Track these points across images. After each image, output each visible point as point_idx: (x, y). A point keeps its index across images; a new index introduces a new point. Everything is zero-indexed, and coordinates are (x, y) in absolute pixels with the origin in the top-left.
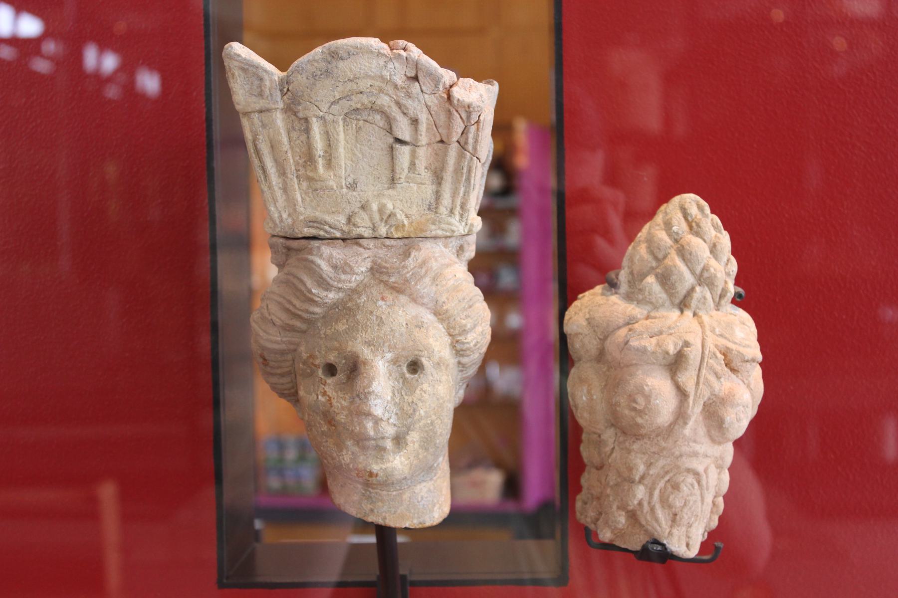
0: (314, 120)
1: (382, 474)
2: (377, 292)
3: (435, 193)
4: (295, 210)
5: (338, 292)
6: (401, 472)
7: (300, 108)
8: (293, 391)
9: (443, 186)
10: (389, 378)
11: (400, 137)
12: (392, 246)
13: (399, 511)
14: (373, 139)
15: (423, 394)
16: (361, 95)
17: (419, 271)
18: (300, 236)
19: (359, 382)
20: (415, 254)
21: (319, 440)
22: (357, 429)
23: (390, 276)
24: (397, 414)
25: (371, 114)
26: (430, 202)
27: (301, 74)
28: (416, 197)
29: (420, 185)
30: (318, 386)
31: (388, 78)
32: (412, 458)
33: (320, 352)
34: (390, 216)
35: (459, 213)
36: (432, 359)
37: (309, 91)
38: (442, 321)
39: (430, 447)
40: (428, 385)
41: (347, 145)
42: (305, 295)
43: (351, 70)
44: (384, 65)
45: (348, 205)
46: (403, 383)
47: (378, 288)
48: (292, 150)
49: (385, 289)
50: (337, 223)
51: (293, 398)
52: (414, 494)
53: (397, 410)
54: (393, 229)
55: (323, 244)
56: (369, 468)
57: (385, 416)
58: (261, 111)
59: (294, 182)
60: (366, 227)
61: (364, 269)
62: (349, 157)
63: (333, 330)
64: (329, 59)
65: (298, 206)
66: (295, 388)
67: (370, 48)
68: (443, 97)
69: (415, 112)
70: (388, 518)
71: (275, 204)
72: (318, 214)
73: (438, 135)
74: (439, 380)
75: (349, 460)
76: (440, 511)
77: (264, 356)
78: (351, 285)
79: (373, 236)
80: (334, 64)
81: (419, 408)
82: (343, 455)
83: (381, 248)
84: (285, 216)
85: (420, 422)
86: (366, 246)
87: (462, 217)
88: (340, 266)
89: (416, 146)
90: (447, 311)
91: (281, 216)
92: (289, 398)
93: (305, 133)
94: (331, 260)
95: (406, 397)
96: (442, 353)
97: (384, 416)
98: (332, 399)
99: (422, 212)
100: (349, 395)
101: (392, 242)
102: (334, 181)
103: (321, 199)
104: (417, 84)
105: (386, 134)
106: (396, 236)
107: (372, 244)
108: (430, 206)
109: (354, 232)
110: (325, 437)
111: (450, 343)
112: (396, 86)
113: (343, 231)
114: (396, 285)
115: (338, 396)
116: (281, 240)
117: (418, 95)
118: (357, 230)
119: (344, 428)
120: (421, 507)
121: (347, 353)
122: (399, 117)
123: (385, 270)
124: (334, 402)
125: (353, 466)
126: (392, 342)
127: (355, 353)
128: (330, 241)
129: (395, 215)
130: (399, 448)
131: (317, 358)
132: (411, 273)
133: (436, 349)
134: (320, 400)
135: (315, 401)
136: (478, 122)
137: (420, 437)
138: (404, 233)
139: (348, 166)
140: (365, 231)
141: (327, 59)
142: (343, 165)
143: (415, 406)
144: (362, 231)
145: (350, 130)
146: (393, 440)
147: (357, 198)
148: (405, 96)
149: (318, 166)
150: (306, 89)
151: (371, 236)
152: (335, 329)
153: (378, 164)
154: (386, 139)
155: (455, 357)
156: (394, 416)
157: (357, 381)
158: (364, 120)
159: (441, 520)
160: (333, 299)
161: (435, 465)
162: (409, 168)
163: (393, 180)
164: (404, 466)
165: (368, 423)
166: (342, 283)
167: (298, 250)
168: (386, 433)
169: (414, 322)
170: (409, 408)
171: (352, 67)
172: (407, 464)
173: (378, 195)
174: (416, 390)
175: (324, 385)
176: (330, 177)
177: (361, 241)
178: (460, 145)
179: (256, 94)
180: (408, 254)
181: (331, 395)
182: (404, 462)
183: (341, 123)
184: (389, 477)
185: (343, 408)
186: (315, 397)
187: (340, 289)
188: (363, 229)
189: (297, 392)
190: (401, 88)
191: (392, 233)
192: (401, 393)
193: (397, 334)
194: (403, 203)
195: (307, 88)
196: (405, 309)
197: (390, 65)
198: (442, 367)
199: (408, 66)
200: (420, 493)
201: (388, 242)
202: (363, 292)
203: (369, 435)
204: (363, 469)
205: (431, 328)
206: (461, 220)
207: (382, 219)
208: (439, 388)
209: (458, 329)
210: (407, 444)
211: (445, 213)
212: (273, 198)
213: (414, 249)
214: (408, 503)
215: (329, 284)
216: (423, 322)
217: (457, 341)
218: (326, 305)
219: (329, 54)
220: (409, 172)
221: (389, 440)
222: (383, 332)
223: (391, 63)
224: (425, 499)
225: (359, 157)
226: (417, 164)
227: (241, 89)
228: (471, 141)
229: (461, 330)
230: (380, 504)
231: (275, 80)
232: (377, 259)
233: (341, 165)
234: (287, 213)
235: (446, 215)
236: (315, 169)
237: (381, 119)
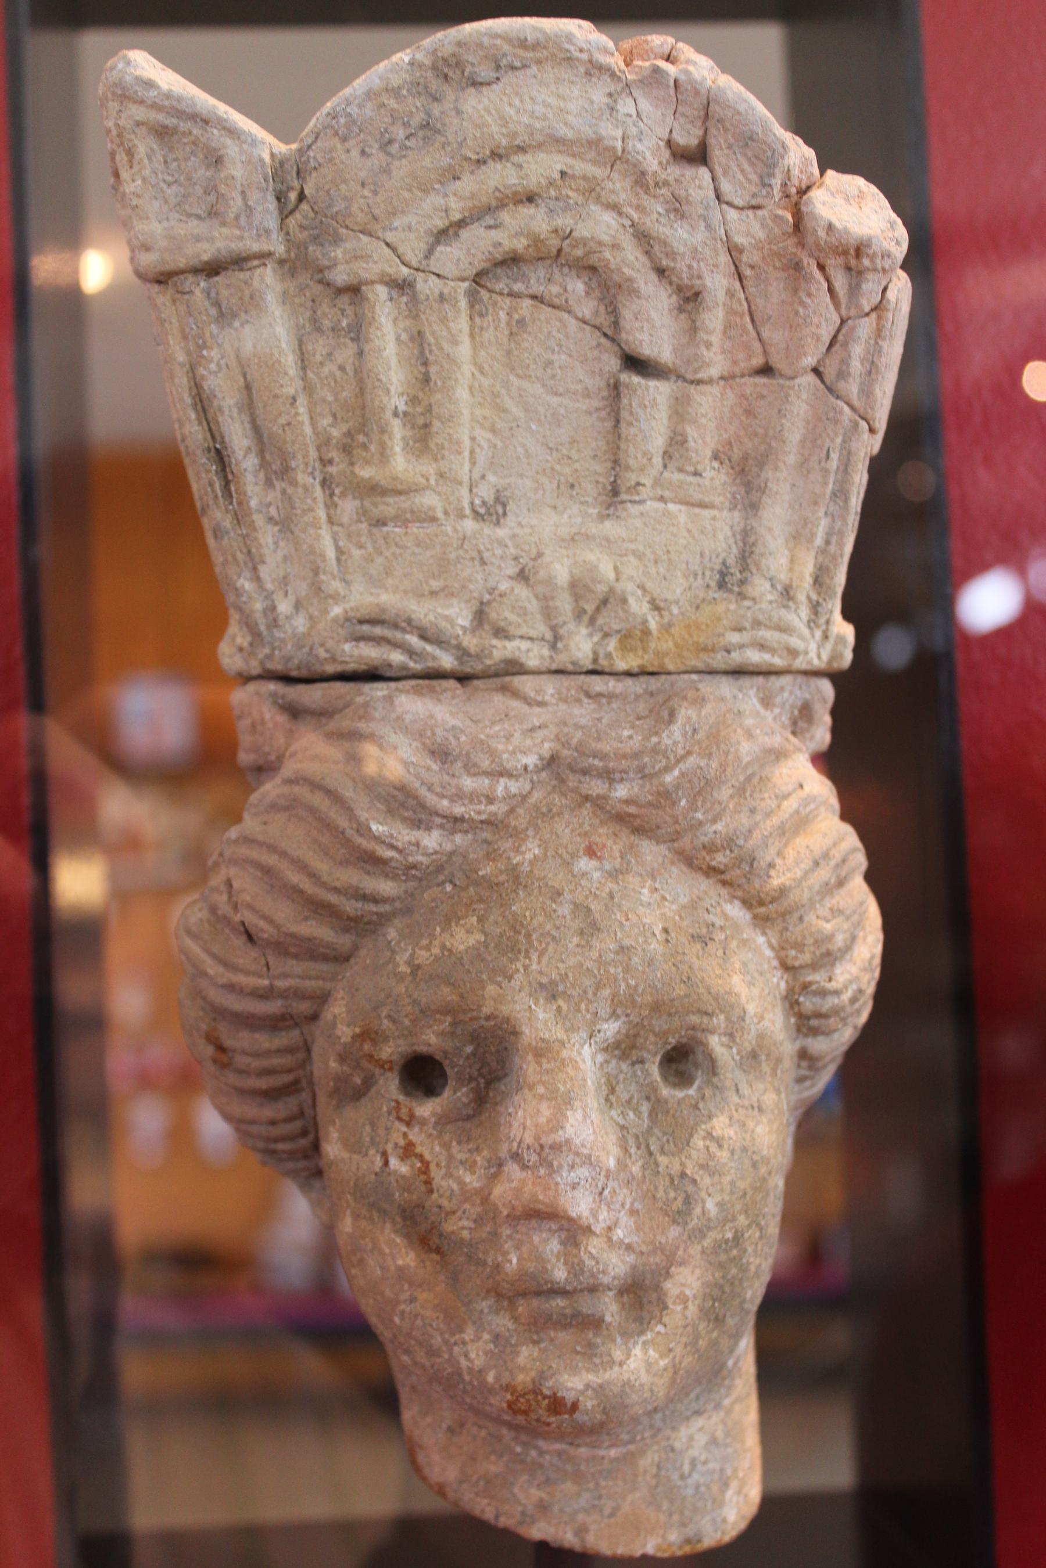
0: (382, 291)
1: (589, 1404)
2: (573, 831)
3: (738, 537)
4: (317, 589)
5: (452, 834)
6: (647, 1395)
7: (339, 253)
8: (304, 1142)
9: (766, 514)
10: (607, 1100)
11: (646, 351)
12: (611, 696)
13: (626, 1508)
14: (561, 359)
15: (713, 1148)
16: (526, 210)
17: (702, 764)
18: (330, 669)
19: (520, 1113)
20: (690, 712)
21: (388, 1293)
22: (510, 1262)
23: (612, 781)
24: (633, 1212)
25: (557, 276)
26: (724, 563)
27: (344, 140)
28: (685, 547)
29: (697, 510)
30: (387, 1129)
31: (619, 145)
32: (679, 1350)
33: (394, 1021)
34: (605, 602)
35: (809, 598)
36: (738, 1040)
37: (366, 193)
38: (762, 922)
39: (728, 1314)
40: (727, 1120)
41: (482, 379)
42: (347, 842)
43: (504, 122)
44: (608, 105)
45: (478, 568)
46: (653, 1114)
47: (575, 820)
48: (310, 396)
49: (597, 821)
50: (443, 624)
51: (301, 1164)
52: (671, 1455)
53: (635, 1200)
54: (612, 645)
55: (401, 691)
56: (550, 1383)
57: (601, 1218)
58: (212, 269)
59: (314, 500)
60: (531, 639)
61: (531, 760)
62: (485, 418)
63: (436, 951)
64: (434, 87)
65: (325, 573)
66: (311, 1137)
67: (567, 46)
68: (781, 218)
69: (695, 265)
70: (593, 1527)
71: (255, 569)
72: (388, 599)
73: (757, 346)
74: (756, 1105)
75: (483, 1358)
76: (741, 1498)
77: (217, 1038)
78: (493, 808)
79: (554, 667)
80: (448, 104)
81: (703, 1194)
82: (464, 1343)
83: (579, 701)
84: (284, 607)
85: (704, 1236)
86: (532, 694)
87: (816, 613)
88: (458, 750)
89: (692, 382)
90: (783, 891)
91: (273, 608)
92: (291, 1165)
93: (352, 339)
94: (429, 733)
95: (663, 1160)
96: (766, 1023)
97: (598, 1221)
98: (433, 1167)
99: (701, 594)
100: (485, 1153)
101: (612, 685)
102: (439, 494)
103: (398, 551)
104: (703, 172)
105: (599, 345)
106: (621, 665)
107: (551, 691)
108: (723, 575)
109: (495, 652)
110: (406, 1287)
111: (784, 993)
112: (641, 180)
113: (462, 653)
114: (632, 810)
115: (450, 1158)
116: (272, 686)
117: (707, 208)
118: (505, 648)
119: (470, 1257)
120: (690, 1491)
121: (483, 1022)
122: (648, 284)
123: (596, 762)
124: (437, 1175)
125: (497, 1379)
126: (623, 986)
127: (508, 1020)
128: (421, 682)
129: (624, 601)
130: (640, 1320)
131: (386, 1039)
132: (676, 773)
133: (751, 1009)
134: (395, 1171)
135: (376, 1174)
136: (878, 308)
137: (703, 1284)
138: (646, 657)
139: (479, 446)
140: (528, 651)
141: (426, 87)
142: (467, 444)
143: (690, 1189)
144: (519, 649)
145: (492, 329)
146: (621, 1293)
147: (506, 546)
148: (668, 211)
149: (389, 443)
150: (359, 188)
151: (546, 664)
152: (443, 947)
153: (573, 442)
154: (599, 359)
155: (794, 1035)
156: (624, 1219)
157: (510, 1110)
158: (534, 297)
159: (743, 1525)
160: (436, 852)
161: (730, 1363)
162: (665, 453)
163: (615, 492)
164: (656, 1375)
165: (546, 1241)
166: (466, 802)
167: (323, 714)
168: (604, 1272)
169: (685, 923)
170: (672, 1195)
171: (507, 108)
172: (665, 1370)
173: (573, 539)
174: (691, 1135)
175: (408, 1124)
176: (427, 480)
177: (517, 681)
178: (823, 381)
179: (199, 212)
180: (665, 714)
181: (427, 1156)
182: (657, 1362)
183: (463, 303)
184: (612, 1413)
185: (466, 1196)
186: (379, 1162)
187: (457, 820)
188: (525, 645)
189: (316, 1147)
190: (657, 184)
191: (609, 656)
192: (648, 1146)
193: (636, 960)
194: (646, 566)
195: (363, 185)
196: (657, 885)
197: (626, 106)
198: (764, 1064)
199: (680, 108)
200: (688, 1448)
201: (598, 684)
202: (530, 832)
203: (552, 1282)
204: (531, 1387)
205: (733, 944)
206: (811, 623)
207: (579, 614)
208: (759, 1129)
209: (812, 949)
210: (666, 1308)
211: (770, 597)
212: (249, 552)
213: (685, 698)
214: (654, 1482)
215: (422, 806)
216: (713, 925)
217: (805, 987)
218: (413, 872)
219: (434, 67)
220: (665, 466)
221: (611, 1294)
222: (595, 955)
223: (630, 101)
224: (699, 1467)
225: (515, 420)
226: (690, 439)
227: (156, 198)
228: (856, 366)
229: (818, 953)
230: (569, 1486)
231: (262, 160)
232: (571, 730)
233: (458, 442)
234: (292, 598)
235: (771, 602)
236: (384, 455)
237: (587, 294)
